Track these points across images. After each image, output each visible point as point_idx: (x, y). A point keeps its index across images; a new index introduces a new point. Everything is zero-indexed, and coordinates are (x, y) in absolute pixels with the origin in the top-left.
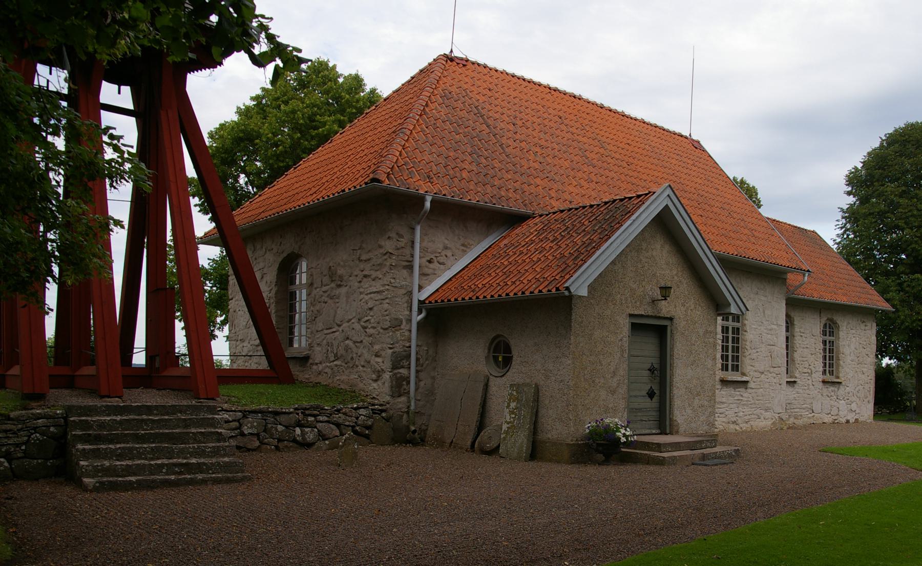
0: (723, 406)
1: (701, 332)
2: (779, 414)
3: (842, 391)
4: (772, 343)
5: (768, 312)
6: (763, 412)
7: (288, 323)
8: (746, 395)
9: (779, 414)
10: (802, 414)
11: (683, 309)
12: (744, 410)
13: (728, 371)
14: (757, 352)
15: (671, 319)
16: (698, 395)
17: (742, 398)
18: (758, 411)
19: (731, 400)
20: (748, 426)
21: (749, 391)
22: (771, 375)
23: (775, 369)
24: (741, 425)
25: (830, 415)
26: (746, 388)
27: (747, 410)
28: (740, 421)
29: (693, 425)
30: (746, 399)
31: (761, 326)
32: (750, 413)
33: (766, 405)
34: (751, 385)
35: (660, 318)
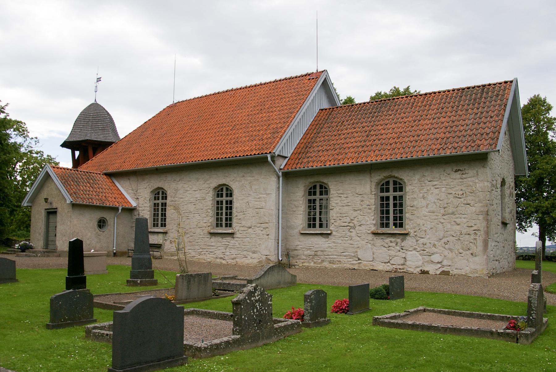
0: (212, 248)
1: (66, 211)
2: (266, 256)
3: (409, 242)
4: (259, 207)
5: (253, 187)
6: (250, 254)
7: (153, 221)
8: (232, 242)
9: (266, 256)
10: (341, 260)
11: (60, 204)
12: (231, 251)
13: (222, 227)
14: (244, 214)
15: (57, 208)
16: (65, 236)
17: (229, 244)
18: (245, 253)
19: (219, 244)
20: (234, 261)
21: (236, 239)
22: (258, 229)
23: (262, 224)
24: (228, 261)
25: (389, 264)
26: (234, 238)
27: (233, 251)
28: (226, 258)
29: (63, 247)
30: (232, 244)
31: (248, 197)
32: (238, 253)
33: (253, 249)
34: (238, 235)
35: (52, 209)
